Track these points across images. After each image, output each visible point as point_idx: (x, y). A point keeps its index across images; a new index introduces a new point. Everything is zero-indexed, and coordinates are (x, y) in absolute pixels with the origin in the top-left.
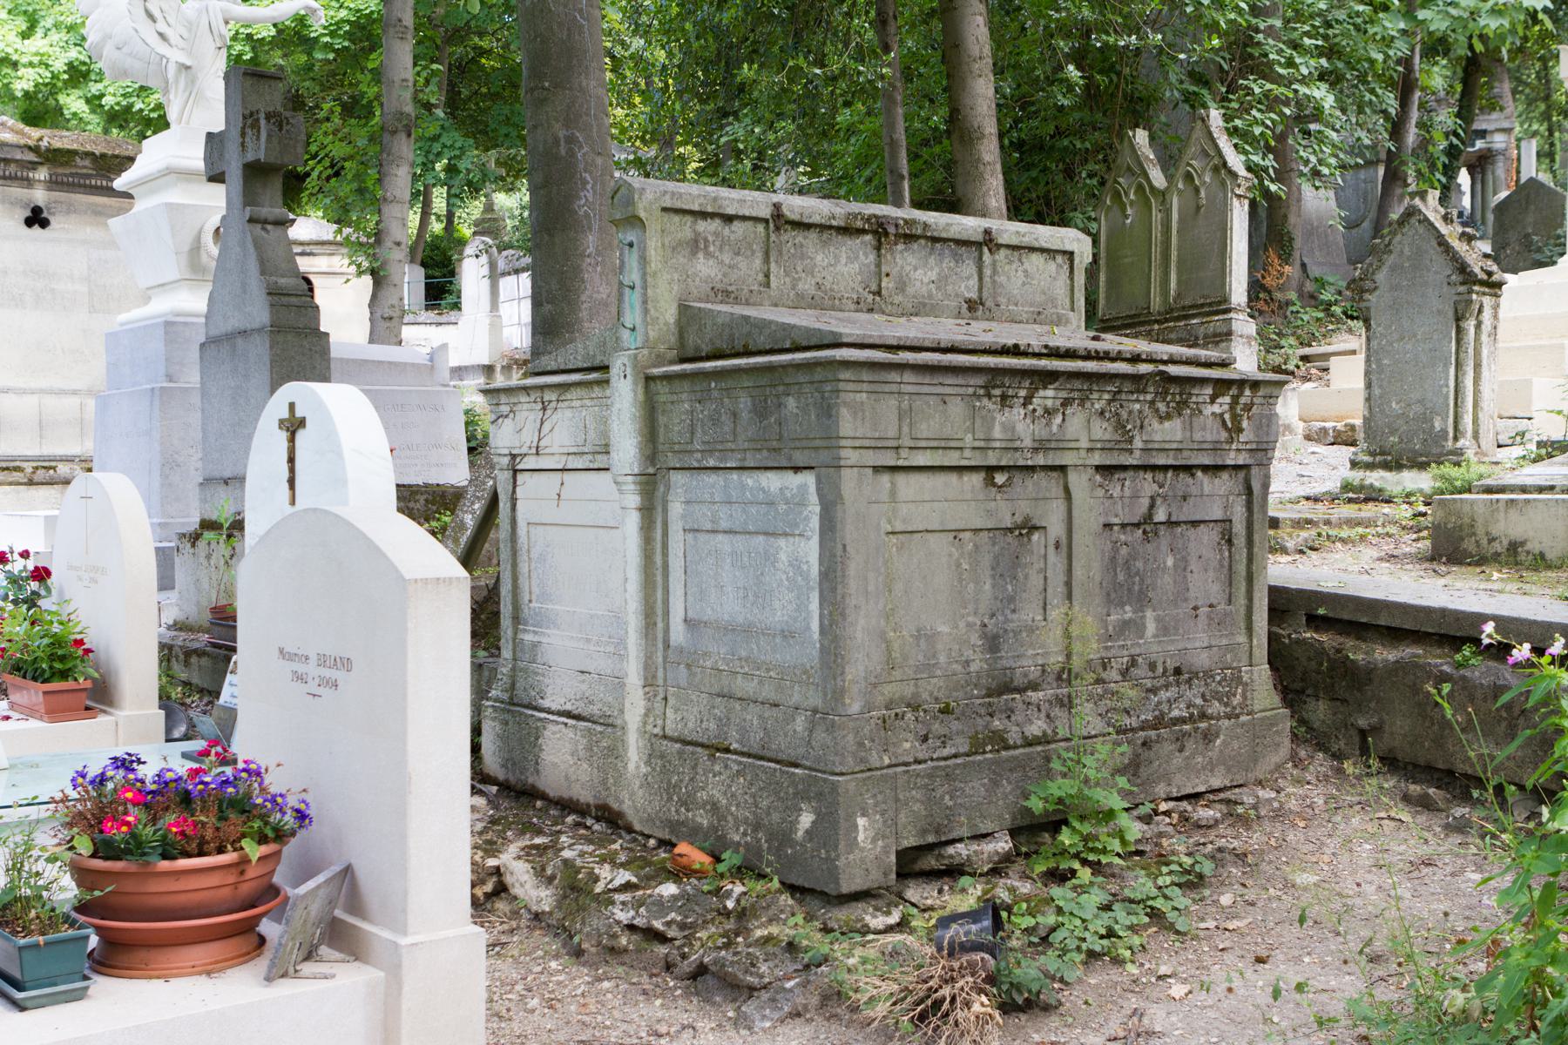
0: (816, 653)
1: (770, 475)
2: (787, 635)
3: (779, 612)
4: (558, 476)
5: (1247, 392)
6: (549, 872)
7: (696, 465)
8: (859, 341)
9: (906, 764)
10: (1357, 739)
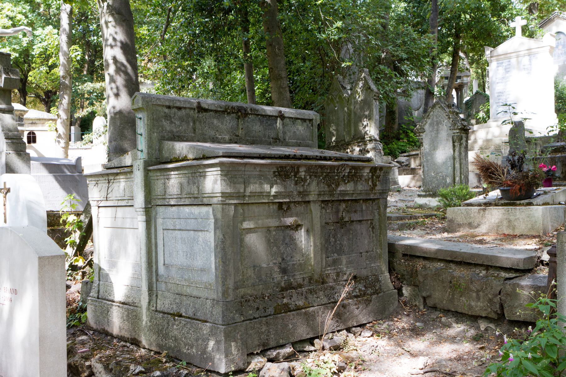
0: (214, 277)
1: (195, 207)
2: (202, 270)
3: (199, 263)
4: (114, 209)
5: (378, 171)
6: (110, 367)
7: (167, 204)
8: (229, 154)
9: (251, 320)
10: (422, 300)
